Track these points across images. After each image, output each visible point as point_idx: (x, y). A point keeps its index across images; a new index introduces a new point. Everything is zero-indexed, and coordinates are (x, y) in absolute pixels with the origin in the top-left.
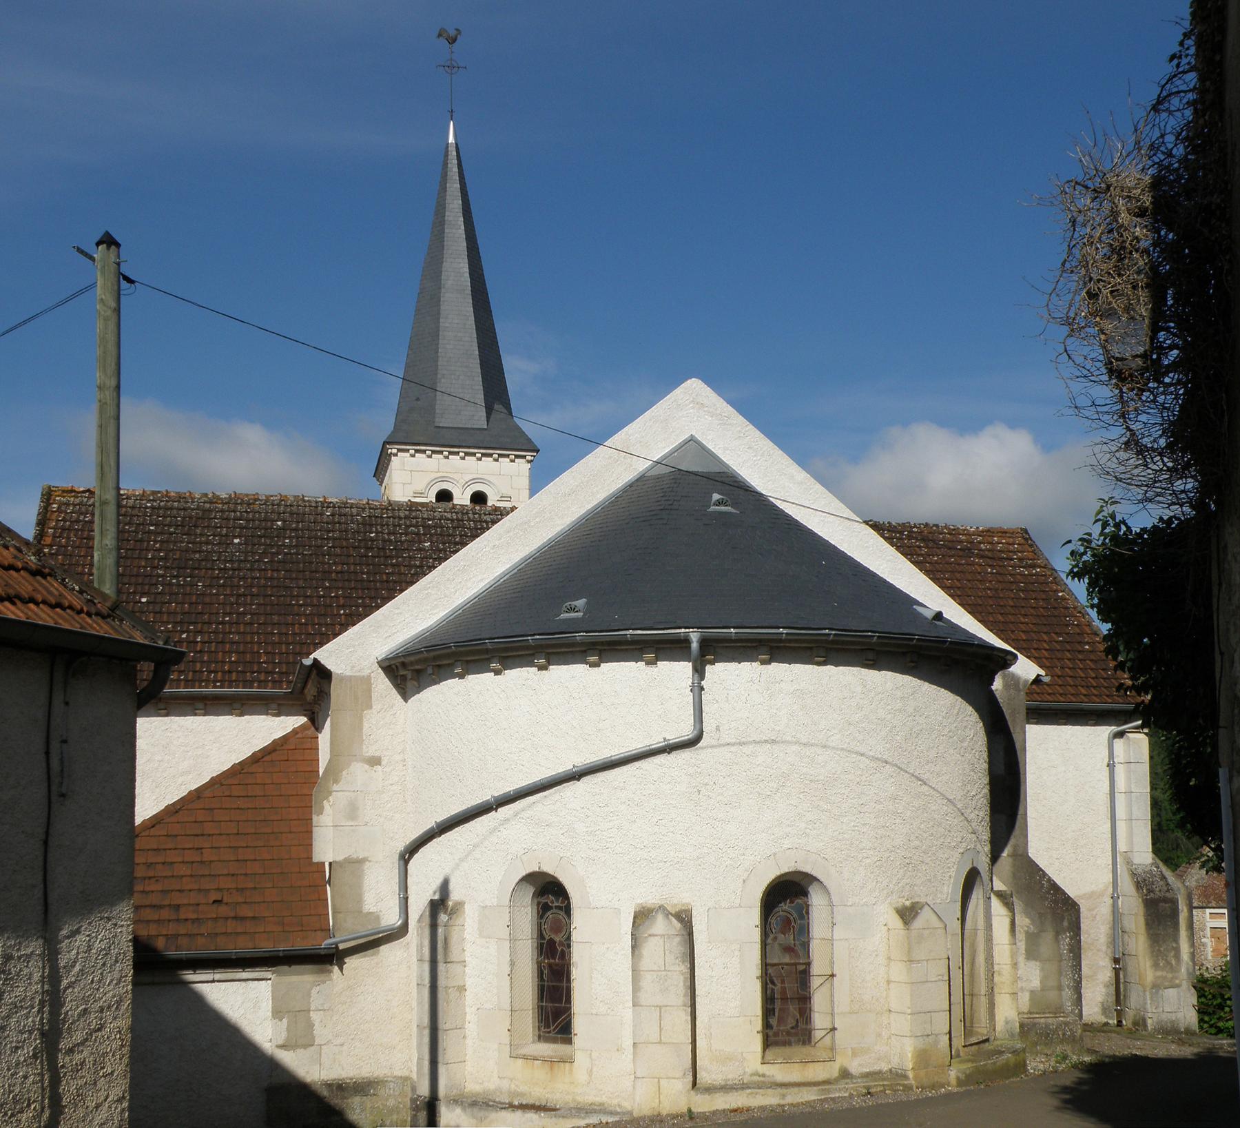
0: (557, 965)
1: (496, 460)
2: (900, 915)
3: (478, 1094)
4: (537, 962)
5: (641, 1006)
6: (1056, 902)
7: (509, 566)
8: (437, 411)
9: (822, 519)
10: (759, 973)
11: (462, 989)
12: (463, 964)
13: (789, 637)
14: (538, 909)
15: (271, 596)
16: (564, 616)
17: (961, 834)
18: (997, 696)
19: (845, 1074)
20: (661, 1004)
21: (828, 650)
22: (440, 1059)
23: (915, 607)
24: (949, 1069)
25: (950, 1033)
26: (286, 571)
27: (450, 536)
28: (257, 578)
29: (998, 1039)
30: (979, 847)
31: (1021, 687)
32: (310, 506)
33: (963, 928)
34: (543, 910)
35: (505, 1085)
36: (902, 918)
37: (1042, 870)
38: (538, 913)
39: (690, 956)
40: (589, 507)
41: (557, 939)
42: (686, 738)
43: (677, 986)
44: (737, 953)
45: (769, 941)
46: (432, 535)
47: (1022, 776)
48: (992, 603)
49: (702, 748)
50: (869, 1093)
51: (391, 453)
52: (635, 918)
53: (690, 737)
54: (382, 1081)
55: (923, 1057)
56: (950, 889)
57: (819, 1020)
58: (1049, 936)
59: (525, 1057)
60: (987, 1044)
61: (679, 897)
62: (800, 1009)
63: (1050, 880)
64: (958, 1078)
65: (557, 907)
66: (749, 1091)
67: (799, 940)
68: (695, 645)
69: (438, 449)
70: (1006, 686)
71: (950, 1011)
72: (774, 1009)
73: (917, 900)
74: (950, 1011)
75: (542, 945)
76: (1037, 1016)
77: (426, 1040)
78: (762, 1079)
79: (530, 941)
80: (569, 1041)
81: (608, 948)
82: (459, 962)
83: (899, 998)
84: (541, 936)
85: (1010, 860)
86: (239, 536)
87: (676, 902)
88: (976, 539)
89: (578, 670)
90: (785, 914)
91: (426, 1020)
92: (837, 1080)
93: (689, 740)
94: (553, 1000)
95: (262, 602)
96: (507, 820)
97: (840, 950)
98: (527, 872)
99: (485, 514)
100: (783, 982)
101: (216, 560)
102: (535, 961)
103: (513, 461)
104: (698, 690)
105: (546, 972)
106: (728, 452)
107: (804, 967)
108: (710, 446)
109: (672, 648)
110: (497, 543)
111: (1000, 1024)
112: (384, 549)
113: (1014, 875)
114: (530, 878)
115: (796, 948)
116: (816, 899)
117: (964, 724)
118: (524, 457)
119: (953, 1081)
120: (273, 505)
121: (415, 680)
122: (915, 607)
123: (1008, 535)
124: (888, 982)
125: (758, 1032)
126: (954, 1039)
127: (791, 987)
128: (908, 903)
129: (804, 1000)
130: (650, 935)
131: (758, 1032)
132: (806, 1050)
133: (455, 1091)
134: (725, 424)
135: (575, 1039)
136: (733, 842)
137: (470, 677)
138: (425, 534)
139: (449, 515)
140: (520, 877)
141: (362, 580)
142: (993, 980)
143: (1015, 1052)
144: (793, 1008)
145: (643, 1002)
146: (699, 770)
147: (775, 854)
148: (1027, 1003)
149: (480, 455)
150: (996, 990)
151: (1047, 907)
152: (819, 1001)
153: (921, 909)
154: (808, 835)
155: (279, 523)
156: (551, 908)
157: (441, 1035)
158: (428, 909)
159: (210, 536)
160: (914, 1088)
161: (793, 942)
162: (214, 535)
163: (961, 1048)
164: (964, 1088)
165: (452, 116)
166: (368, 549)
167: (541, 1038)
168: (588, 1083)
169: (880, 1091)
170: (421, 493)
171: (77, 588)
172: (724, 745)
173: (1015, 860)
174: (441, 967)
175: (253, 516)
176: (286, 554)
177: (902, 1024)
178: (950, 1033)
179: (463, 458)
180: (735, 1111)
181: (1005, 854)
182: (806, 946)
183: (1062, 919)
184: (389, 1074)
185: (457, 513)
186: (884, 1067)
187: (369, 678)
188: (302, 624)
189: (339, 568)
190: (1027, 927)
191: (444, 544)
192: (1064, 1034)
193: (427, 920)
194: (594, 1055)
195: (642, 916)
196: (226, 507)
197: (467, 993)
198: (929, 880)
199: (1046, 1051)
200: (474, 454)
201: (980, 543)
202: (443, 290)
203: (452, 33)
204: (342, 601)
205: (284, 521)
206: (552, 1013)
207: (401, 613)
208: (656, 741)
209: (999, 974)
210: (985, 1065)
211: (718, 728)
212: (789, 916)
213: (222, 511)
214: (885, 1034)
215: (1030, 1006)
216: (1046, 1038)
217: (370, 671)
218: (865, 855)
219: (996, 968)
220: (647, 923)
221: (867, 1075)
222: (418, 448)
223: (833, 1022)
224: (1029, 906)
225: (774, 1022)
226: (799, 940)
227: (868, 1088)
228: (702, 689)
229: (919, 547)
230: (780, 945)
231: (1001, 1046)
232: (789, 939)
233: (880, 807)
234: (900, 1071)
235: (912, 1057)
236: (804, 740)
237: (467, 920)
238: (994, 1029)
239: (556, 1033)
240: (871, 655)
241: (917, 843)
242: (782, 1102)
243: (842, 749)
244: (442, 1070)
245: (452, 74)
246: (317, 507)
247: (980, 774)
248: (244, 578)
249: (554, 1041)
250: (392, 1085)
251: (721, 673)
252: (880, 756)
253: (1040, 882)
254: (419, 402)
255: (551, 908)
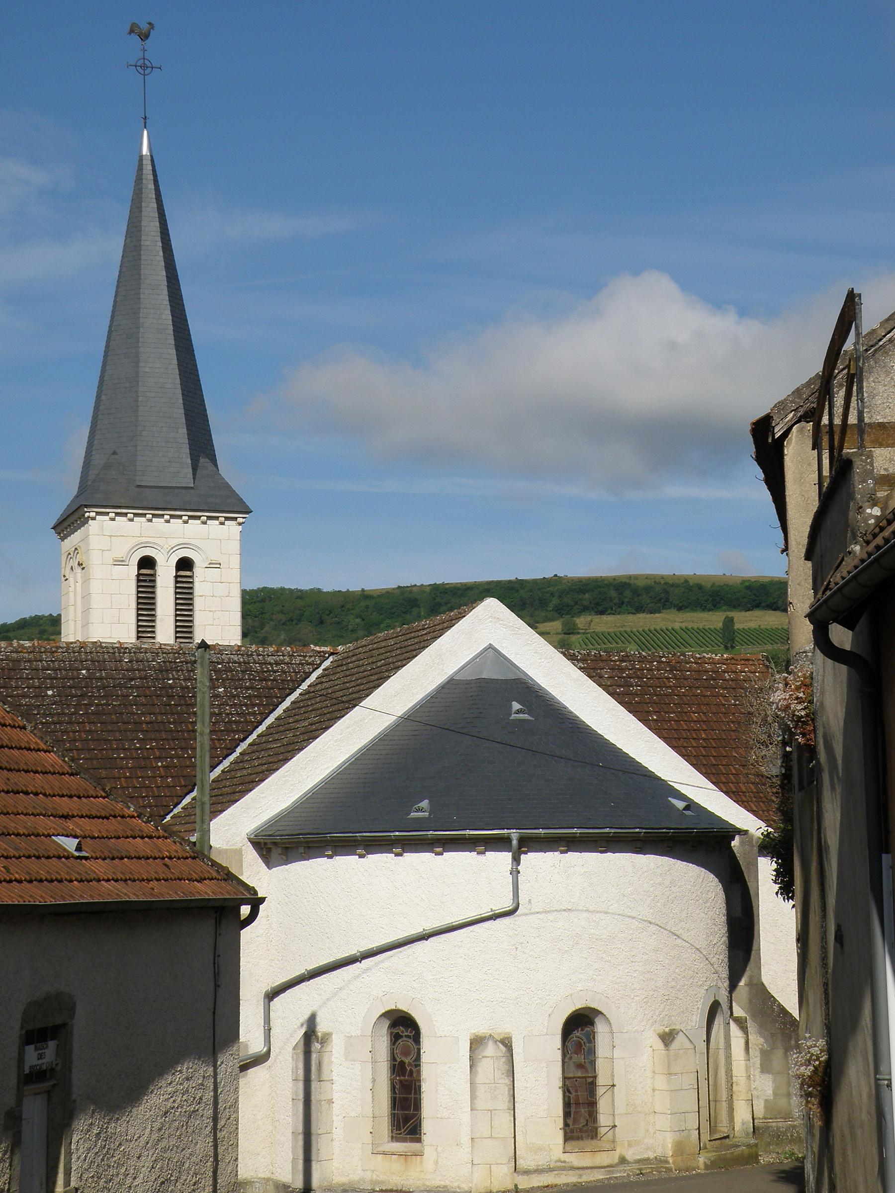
0: (406, 1081)
1: (204, 523)
2: (661, 1039)
3: (344, 1184)
4: (391, 1080)
5: (477, 1110)
6: (784, 1024)
7: (348, 756)
8: (138, 468)
9: (593, 708)
10: (561, 1084)
11: (331, 1102)
12: (331, 1082)
13: (582, 835)
14: (391, 1037)
15: (94, 749)
16: (414, 815)
17: (706, 975)
18: (735, 851)
19: (623, 1161)
20: (492, 1109)
21: (608, 842)
22: (314, 1157)
23: (669, 799)
24: (698, 1157)
25: (699, 1128)
26: (101, 723)
27: (240, 680)
28: (77, 731)
29: (736, 1138)
30: (720, 984)
31: (754, 844)
32: (108, 653)
33: (708, 1049)
34: (395, 1038)
35: (368, 1176)
36: (663, 1041)
37: (773, 997)
38: (391, 1041)
39: (512, 1073)
40: (410, 705)
41: (407, 1061)
42: (508, 909)
43: (503, 1094)
44: (545, 1069)
45: (566, 1060)
46: (223, 680)
47: (755, 918)
48: (734, 737)
49: (518, 916)
50: (641, 1173)
51: (89, 517)
52: (471, 1044)
53: (510, 908)
54: (250, 1182)
55: (679, 1148)
56: (698, 1018)
57: (603, 1120)
58: (779, 1053)
59: (384, 1153)
60: (728, 1140)
61: (502, 1028)
62: (589, 1111)
63: (780, 1005)
64: (705, 1163)
65: (406, 1036)
66: (555, 1172)
67: (588, 1059)
68: (515, 842)
69: (140, 512)
70: (742, 843)
71: (699, 1112)
72: (570, 1112)
73: (673, 1027)
74: (699, 1112)
75: (394, 1065)
76: (771, 1121)
77: (301, 1143)
78: (564, 1164)
79: (386, 1063)
80: (419, 1140)
81: (450, 1067)
82: (328, 1081)
83: (662, 1103)
84: (393, 1058)
85: (747, 988)
86: (51, 688)
87: (500, 1031)
88: (721, 667)
89: (426, 858)
90: (577, 1039)
91: (300, 1128)
92: (617, 1165)
93: (510, 910)
94: (403, 1108)
95: (88, 756)
96: (368, 969)
97: (619, 1066)
98: (386, 1010)
99: (269, 656)
100: (576, 1091)
101: (37, 714)
102: (389, 1079)
103: (222, 524)
104: (515, 873)
105: (397, 1087)
106: (518, 656)
107: (592, 1079)
108: (504, 652)
109: (499, 843)
110: (339, 737)
111: (738, 1126)
112: (183, 696)
113: (750, 1002)
114: (387, 1014)
115: (586, 1065)
116: (600, 1027)
117: (708, 889)
118: (235, 519)
119: (702, 1166)
120: (74, 653)
121: (284, 855)
122: (669, 799)
123: (751, 662)
124: (654, 1090)
125: (560, 1129)
126: (701, 1135)
127: (583, 1095)
128: (667, 1030)
129: (592, 1104)
130: (483, 1057)
131: (560, 1129)
132: (594, 1142)
133: (326, 1183)
134: (517, 634)
135: (424, 1137)
136: (541, 986)
137: (338, 858)
138: (217, 680)
139: (236, 658)
140: (380, 1013)
141: (171, 731)
142: (732, 1089)
143: (749, 1146)
144: (584, 1111)
145: (478, 1107)
146: (516, 933)
147: (571, 995)
148: (763, 1110)
149: (187, 518)
150: (734, 1097)
151: (778, 1028)
152: (603, 1105)
153: (677, 1034)
154: (595, 980)
155: (84, 672)
156: (401, 1037)
157: (313, 1138)
158: (302, 1039)
159: (24, 688)
160: (673, 1169)
161: (583, 1060)
162: (29, 688)
163: (707, 1142)
164: (709, 1171)
165: (145, 123)
166: (171, 697)
167: (393, 1139)
168: (435, 1171)
169: (649, 1172)
170: (122, 561)
171: (210, 864)
172: (534, 913)
173: (750, 989)
174: (314, 1085)
175: (59, 665)
176: (97, 705)
177: (663, 1122)
178: (699, 1128)
179: (168, 521)
180: (547, 1186)
181: (742, 983)
182: (593, 1063)
183: (790, 1038)
184: (255, 1176)
185: (242, 655)
186: (651, 1155)
187: (240, 851)
188: (126, 778)
189: (148, 719)
190: (762, 1045)
191: (236, 689)
192: (792, 1136)
193: (301, 1048)
194: (439, 1149)
195: (477, 1043)
196: (31, 656)
197: (334, 1105)
198: (683, 1012)
199: (777, 1150)
200: (180, 517)
201: (724, 672)
202: (142, 330)
203: (144, 27)
204: (158, 754)
205: (88, 670)
206: (403, 1118)
207: (265, 797)
208: (485, 911)
209: (737, 1085)
210: (725, 1154)
211: (530, 901)
212: (581, 1040)
213: (29, 661)
214: (652, 1130)
215: (765, 1112)
216: (777, 1139)
217: (241, 845)
218: (636, 994)
219: (734, 1079)
220: (480, 1048)
221: (639, 1161)
222: (119, 511)
223: (614, 1122)
224: (763, 1029)
225: (570, 1122)
226: (588, 1059)
227: (640, 1170)
228: (519, 872)
229: (668, 678)
230: (574, 1062)
231: (739, 1142)
232: (579, 1058)
233: (646, 957)
234: (662, 1158)
235: (672, 1147)
236: (591, 909)
237: (335, 1047)
238: (734, 1129)
239: (406, 1135)
240: (639, 845)
241: (673, 984)
242: (580, 1180)
243: (619, 915)
244: (315, 1166)
245: (144, 75)
246: (114, 653)
247: (720, 926)
248: (65, 732)
249: (404, 1140)
250: (257, 1185)
251: (530, 859)
252: (646, 919)
253: (772, 1007)
254: (116, 457)
255: (401, 1037)
